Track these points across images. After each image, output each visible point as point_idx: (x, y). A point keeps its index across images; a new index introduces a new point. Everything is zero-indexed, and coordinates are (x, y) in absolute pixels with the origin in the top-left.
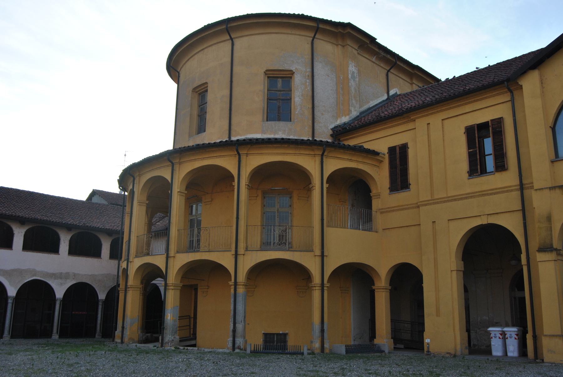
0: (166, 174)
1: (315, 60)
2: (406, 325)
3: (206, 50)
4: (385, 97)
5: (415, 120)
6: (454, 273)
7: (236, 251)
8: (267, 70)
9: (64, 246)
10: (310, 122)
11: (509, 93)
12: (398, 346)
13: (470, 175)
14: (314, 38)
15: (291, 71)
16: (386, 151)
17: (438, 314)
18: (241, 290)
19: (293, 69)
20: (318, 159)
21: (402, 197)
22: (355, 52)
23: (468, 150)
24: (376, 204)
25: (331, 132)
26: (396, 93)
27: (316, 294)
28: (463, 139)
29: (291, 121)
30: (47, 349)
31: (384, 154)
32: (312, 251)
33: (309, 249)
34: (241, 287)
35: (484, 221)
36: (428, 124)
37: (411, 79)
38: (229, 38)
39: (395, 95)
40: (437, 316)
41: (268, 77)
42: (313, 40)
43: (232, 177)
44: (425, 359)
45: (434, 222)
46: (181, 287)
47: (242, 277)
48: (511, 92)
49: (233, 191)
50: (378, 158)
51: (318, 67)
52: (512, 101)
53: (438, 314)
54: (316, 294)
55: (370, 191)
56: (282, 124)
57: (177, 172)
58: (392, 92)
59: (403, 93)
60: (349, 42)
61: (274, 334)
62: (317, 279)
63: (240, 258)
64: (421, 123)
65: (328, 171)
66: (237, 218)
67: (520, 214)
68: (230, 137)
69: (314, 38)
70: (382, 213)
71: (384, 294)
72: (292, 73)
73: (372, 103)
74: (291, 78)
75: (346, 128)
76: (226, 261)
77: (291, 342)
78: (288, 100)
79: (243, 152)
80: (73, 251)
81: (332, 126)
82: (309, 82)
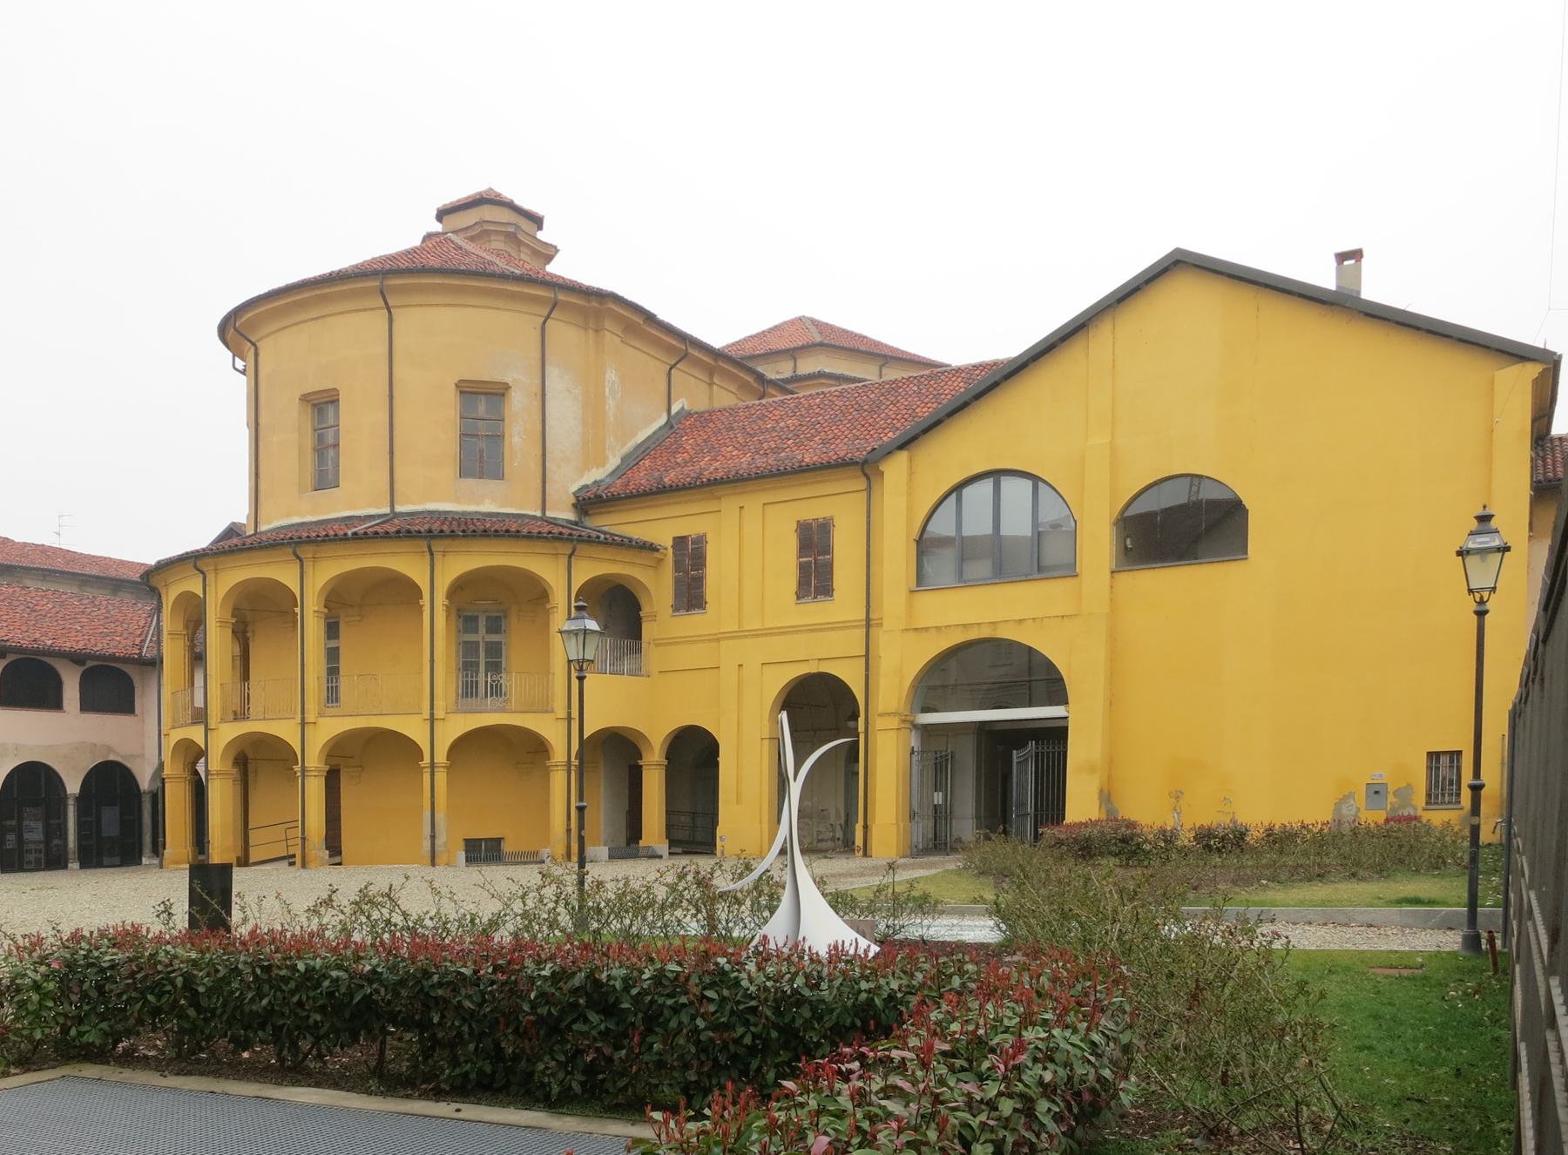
0: (286, 575)
1: (547, 362)
2: (682, 818)
3: (329, 319)
4: (663, 420)
5: (720, 498)
6: (766, 742)
7: (432, 714)
8: (461, 381)
9: (71, 692)
10: (539, 481)
11: (864, 479)
12: (673, 850)
13: (798, 598)
14: (548, 317)
15: (507, 384)
16: (669, 543)
17: (739, 801)
18: (441, 777)
19: (508, 380)
20: (563, 561)
21: (692, 623)
22: (617, 340)
23: (800, 557)
24: (647, 629)
25: (573, 500)
26: (683, 408)
27: (558, 780)
28: (792, 542)
29: (503, 479)
30: (668, 898)
31: (666, 549)
32: (552, 711)
33: (546, 709)
34: (442, 769)
35: (812, 668)
36: (741, 508)
37: (711, 375)
38: (383, 304)
39: (685, 415)
40: (737, 803)
41: (461, 392)
42: (544, 322)
43: (418, 592)
44: (1070, 1030)
45: (740, 666)
46: (328, 772)
47: (441, 757)
48: (868, 478)
49: (421, 613)
50: (656, 555)
51: (553, 373)
52: (869, 489)
53: (739, 801)
54: (558, 780)
55: (639, 608)
56: (490, 485)
57: (311, 572)
58: (675, 409)
59: (696, 409)
60: (608, 324)
61: (481, 840)
62: (559, 754)
63: (438, 726)
64: (729, 505)
65: (579, 580)
66: (432, 661)
67: (863, 661)
68: (392, 506)
69: (548, 317)
70: (657, 645)
71: (657, 772)
72: (506, 387)
73: (641, 436)
74: (503, 395)
75: (601, 497)
76: (414, 729)
77: (507, 847)
78: (497, 438)
79: (438, 546)
80: (88, 705)
81: (574, 488)
82: (537, 404)
